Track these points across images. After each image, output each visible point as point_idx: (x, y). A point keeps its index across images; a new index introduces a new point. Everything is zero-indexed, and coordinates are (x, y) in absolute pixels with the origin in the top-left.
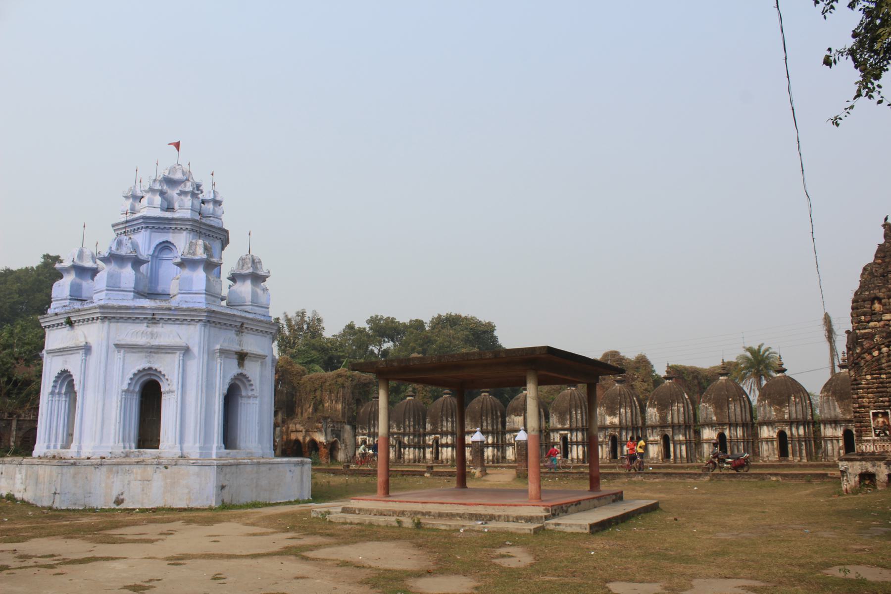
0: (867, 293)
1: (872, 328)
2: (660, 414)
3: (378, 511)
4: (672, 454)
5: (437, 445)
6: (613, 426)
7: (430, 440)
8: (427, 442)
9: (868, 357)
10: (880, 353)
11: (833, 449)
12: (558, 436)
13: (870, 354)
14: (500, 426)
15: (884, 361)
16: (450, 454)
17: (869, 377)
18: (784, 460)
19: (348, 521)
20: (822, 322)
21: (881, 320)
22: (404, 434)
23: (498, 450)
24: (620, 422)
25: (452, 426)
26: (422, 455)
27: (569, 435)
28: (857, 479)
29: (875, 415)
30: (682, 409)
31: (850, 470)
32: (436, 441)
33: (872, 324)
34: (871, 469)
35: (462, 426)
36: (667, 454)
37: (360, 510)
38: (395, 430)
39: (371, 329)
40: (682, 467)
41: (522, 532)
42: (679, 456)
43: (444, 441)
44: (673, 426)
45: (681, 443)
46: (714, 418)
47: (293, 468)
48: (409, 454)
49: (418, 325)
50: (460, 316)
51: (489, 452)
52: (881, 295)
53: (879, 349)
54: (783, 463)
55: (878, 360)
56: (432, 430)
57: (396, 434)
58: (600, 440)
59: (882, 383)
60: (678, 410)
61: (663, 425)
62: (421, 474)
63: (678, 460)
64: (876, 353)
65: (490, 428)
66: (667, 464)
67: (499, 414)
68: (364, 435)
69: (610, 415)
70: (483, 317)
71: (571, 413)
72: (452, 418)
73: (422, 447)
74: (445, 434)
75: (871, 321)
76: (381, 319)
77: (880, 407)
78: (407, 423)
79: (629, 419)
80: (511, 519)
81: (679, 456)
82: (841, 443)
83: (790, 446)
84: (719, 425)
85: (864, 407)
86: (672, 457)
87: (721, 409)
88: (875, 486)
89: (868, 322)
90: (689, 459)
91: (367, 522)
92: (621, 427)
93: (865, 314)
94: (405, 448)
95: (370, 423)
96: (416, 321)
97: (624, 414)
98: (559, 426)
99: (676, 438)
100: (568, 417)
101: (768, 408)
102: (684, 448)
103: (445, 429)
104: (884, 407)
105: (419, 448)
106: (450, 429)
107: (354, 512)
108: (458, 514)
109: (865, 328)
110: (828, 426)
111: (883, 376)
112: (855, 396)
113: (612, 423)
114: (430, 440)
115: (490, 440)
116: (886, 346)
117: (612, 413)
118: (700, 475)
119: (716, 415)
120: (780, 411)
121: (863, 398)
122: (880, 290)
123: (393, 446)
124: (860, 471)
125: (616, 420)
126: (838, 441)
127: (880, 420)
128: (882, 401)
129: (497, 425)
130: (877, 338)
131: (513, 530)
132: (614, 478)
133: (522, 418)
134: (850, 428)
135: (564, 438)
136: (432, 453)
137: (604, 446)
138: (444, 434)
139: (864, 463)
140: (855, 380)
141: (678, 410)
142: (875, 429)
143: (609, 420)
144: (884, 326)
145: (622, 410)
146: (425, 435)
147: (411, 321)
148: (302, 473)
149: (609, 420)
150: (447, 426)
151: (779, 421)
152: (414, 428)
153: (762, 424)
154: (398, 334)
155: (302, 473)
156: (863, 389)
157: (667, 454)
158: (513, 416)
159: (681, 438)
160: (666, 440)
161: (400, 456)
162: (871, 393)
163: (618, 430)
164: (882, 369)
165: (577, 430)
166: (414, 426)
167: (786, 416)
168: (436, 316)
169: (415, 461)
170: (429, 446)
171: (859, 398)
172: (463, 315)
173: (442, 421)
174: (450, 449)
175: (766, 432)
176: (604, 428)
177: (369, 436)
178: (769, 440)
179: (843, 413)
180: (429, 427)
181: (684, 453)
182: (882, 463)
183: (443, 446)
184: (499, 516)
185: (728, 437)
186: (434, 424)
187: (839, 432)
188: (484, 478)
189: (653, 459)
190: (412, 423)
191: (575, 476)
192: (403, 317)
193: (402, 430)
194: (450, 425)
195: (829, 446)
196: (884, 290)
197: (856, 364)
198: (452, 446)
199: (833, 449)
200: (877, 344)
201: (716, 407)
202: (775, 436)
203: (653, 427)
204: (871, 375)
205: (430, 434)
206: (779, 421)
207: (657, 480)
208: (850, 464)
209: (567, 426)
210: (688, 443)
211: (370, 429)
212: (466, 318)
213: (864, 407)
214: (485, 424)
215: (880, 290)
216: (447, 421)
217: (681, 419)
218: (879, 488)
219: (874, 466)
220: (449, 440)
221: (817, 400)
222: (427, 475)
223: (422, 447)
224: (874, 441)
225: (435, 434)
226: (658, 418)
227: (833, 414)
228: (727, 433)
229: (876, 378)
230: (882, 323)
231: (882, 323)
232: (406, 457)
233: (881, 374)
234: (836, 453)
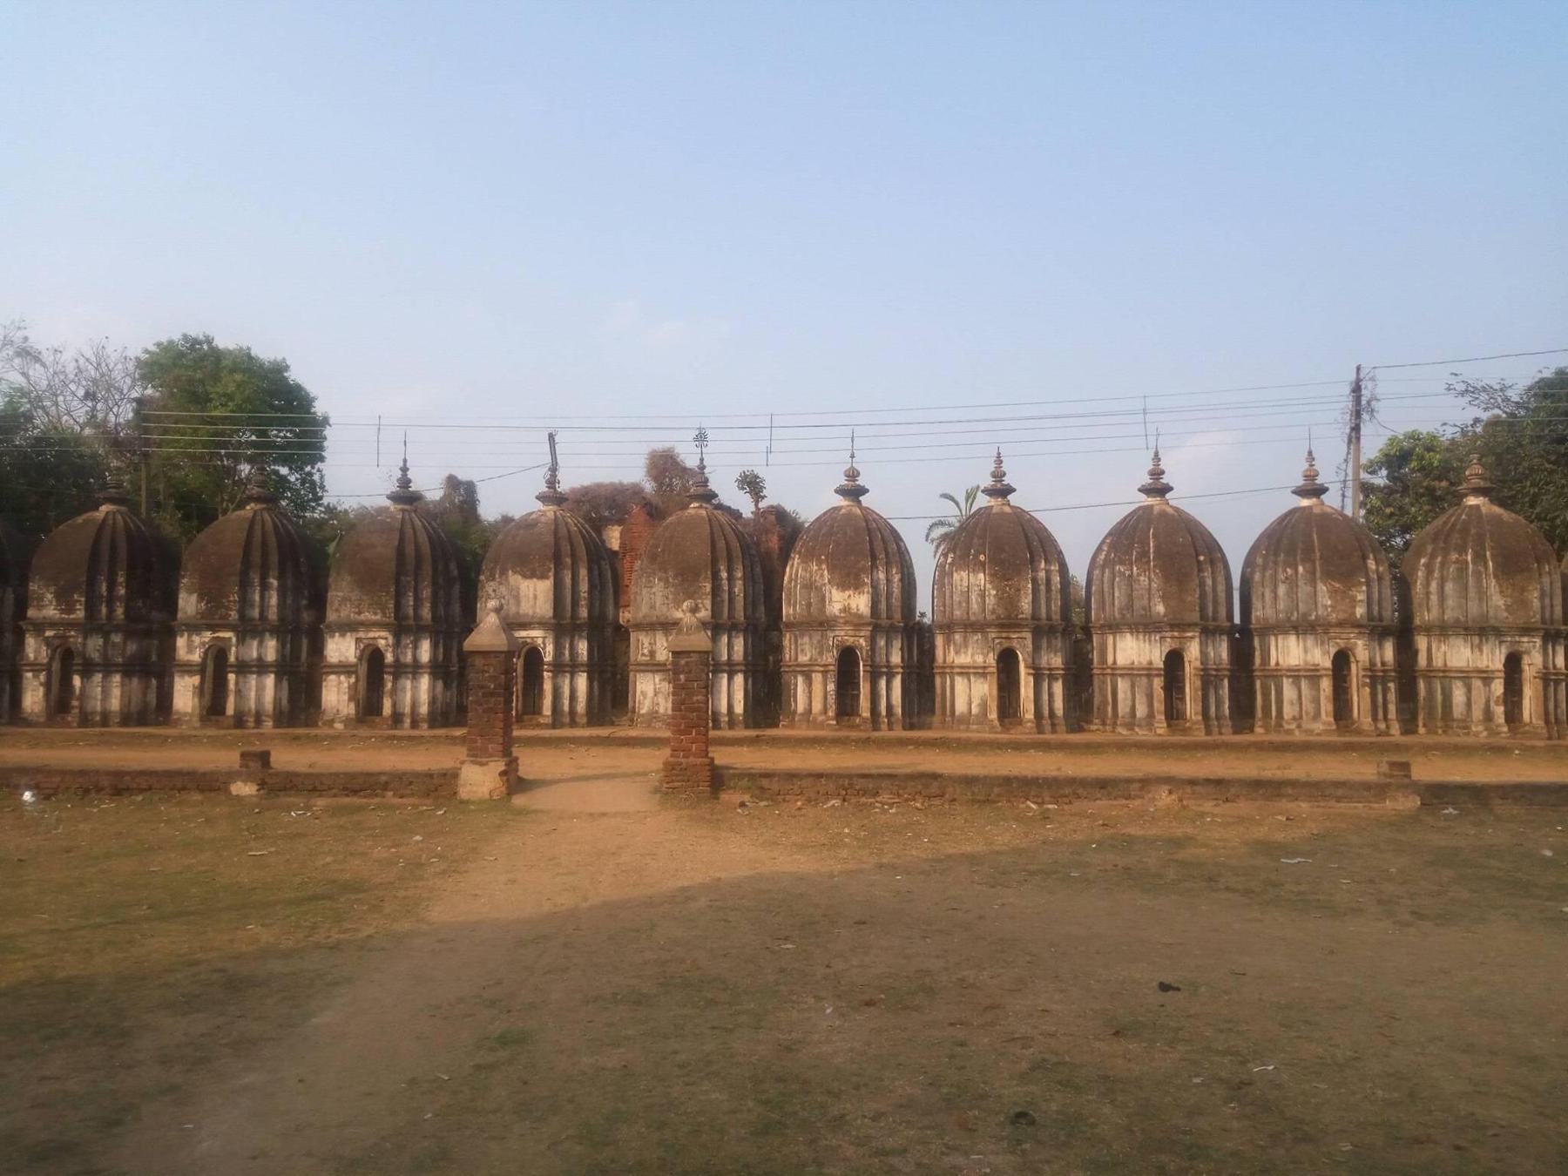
14: (457, 608)
20: (1347, 390)
23: (447, 686)
26: (152, 698)
38: (51, 612)
56: (203, 615)
57: (53, 624)
62: (210, 784)
65: (426, 612)
69: (843, 586)
71: (715, 577)
72: (280, 578)
84: (1173, 627)
101: (1304, 589)
113: (846, 609)
115: (1454, 556)
119: (1164, 598)
129: (448, 604)
136: (200, 690)
137: (817, 678)
138: (248, 629)
149: (838, 601)
158: (514, 579)
163: (866, 631)
165: (732, 628)
166: (129, 600)
167: (1360, 611)
173: (244, 585)
178: (343, 669)
181: (1059, 704)
183: (243, 668)
187: (1493, 658)
193: (80, 614)
195: (1459, 695)
198: (260, 659)
199: (1469, 704)
201: (1167, 578)
202: (1328, 664)
205: (194, 628)
206: (1340, 624)
210: (439, 670)
221: (925, 561)
225: (213, 628)
226: (991, 601)
227: (1474, 609)
234: (1477, 713)
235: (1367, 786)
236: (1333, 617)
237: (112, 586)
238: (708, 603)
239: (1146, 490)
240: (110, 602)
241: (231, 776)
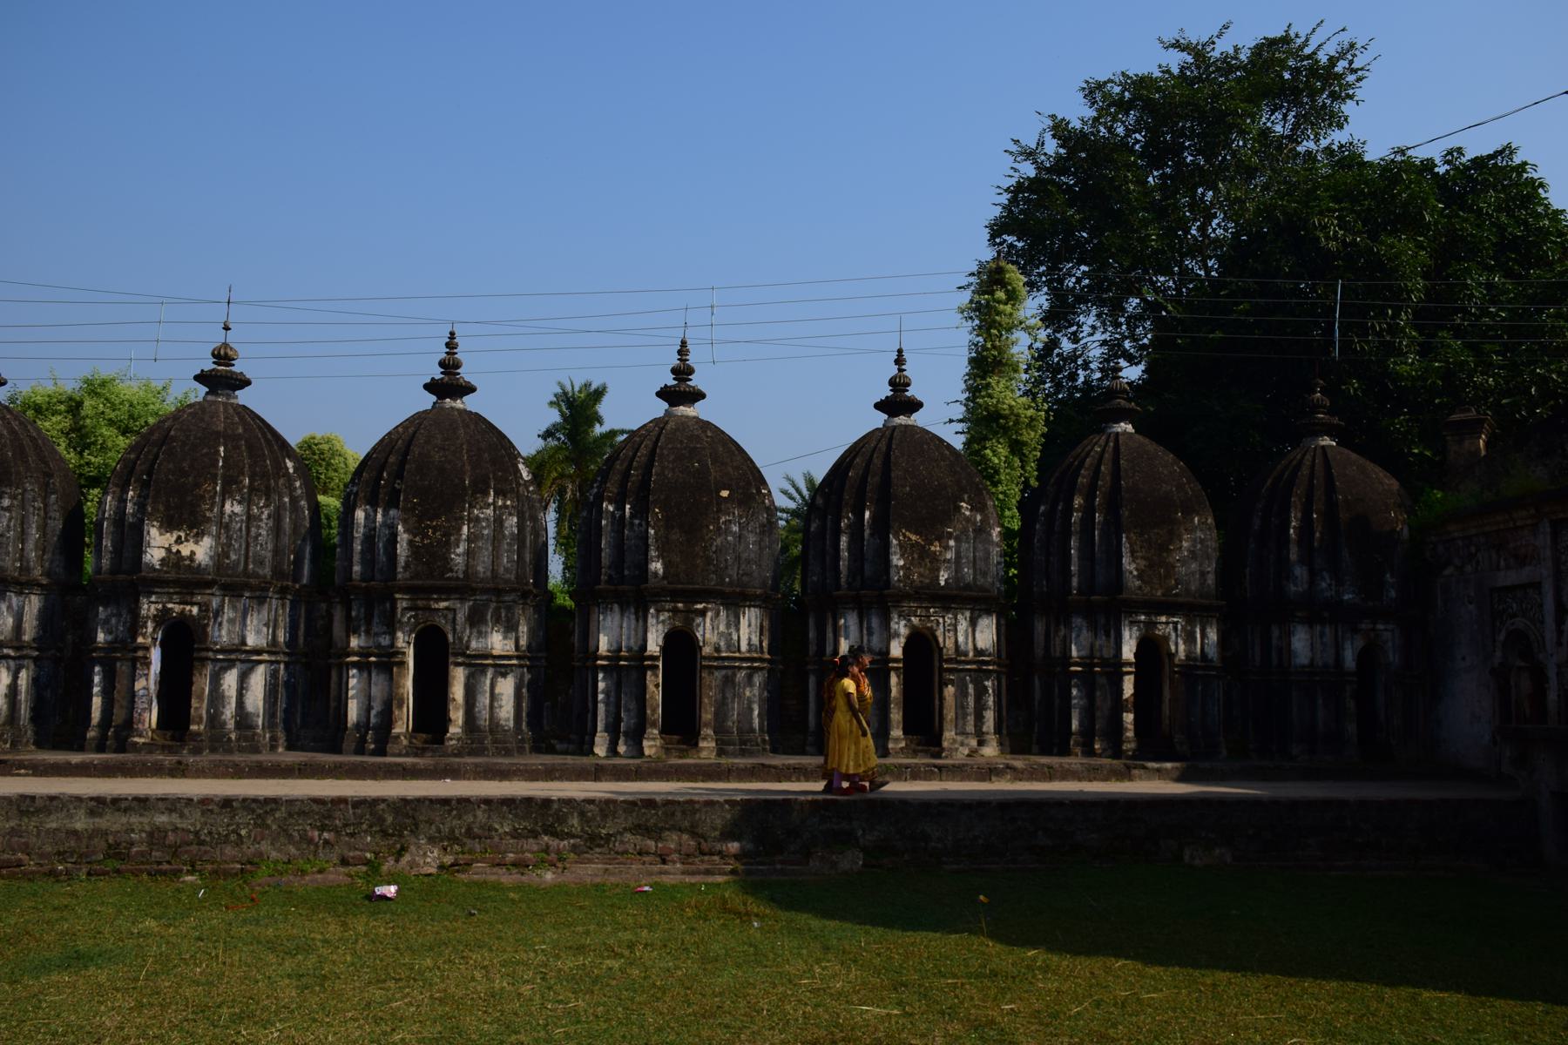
6: (182, 578)
44: (462, 588)
69: (168, 525)
84: (675, 595)
113: (173, 560)
125: (201, 550)
134: (1161, 630)
141: (499, 522)
159: (498, 642)
181: (506, 711)
239: (664, 394)
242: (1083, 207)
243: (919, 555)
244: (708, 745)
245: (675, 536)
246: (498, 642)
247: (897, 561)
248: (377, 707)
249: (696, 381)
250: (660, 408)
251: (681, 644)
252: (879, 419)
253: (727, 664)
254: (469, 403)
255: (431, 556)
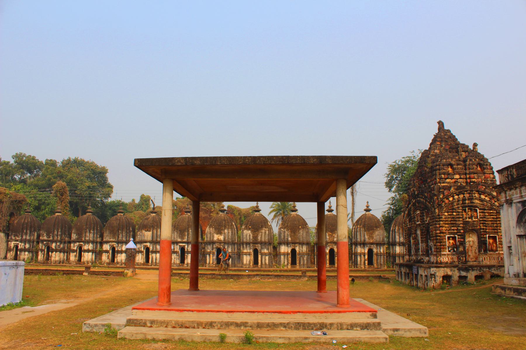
0: (445, 161)
1: (448, 183)
2: (253, 234)
3: (177, 323)
4: (260, 262)
5: (81, 250)
6: (220, 242)
7: (74, 246)
8: (72, 248)
9: (447, 201)
10: (454, 199)
11: (361, 261)
12: (178, 246)
13: (448, 199)
15: (455, 204)
16: (90, 257)
17: (446, 214)
18: (332, 267)
19: (150, 337)
21: (453, 178)
22: (52, 241)
24: (224, 239)
25: (94, 237)
26: (65, 257)
27: (186, 246)
28: (441, 279)
29: (449, 238)
30: (267, 232)
31: (437, 274)
32: (80, 248)
33: (448, 180)
34: (450, 273)
35: (102, 236)
36: (256, 262)
37: (152, 322)
38: (45, 238)
39: (16, 162)
40: (264, 271)
41: (377, 341)
42: (264, 263)
43: (86, 247)
44: (261, 243)
45: (265, 254)
46: (290, 239)
47: (7, 270)
48: (56, 257)
49: (52, 164)
50: (84, 161)
51: (140, 258)
52: (453, 162)
53: (453, 197)
54: (332, 269)
55: (452, 203)
56: (77, 239)
57: (46, 241)
58: (209, 251)
59: (453, 218)
60: (265, 233)
61: (255, 242)
62: (81, 273)
63: (264, 266)
64: (451, 199)
66: (256, 269)
67: (131, 229)
68: (17, 241)
69: (217, 234)
70: (100, 163)
71: (188, 231)
72: (94, 230)
73: (67, 251)
74: (88, 242)
75: (448, 178)
76: (24, 156)
77: (451, 233)
78: (56, 233)
79: (230, 237)
80: (345, 327)
81: (264, 263)
82: (366, 257)
83: (336, 258)
84: (293, 243)
85: (443, 233)
86: (260, 264)
87: (294, 233)
88: (450, 285)
89: (446, 179)
90: (270, 265)
91: (177, 338)
92: (225, 242)
93: (444, 174)
94: (52, 252)
95: (23, 232)
96: (51, 160)
97: (227, 234)
98: (179, 240)
99: (262, 251)
100: (186, 233)
102: (267, 258)
103: (87, 239)
104: (454, 234)
105: (64, 252)
106: (91, 239)
107: (144, 325)
108: (281, 324)
109: (444, 183)
110: (359, 246)
111: (454, 214)
112: (438, 226)
113: (218, 239)
114: (74, 246)
116: (457, 195)
117: (219, 232)
118: (300, 276)
119: (291, 237)
120: (332, 236)
121: (443, 227)
122: (452, 159)
123: (42, 250)
124: (443, 274)
125: (222, 238)
126: (364, 256)
127: (451, 241)
128: (453, 230)
130: (452, 189)
131: (366, 340)
132: (238, 279)
133: (151, 232)
135: (113, 249)
136: (76, 256)
137: (211, 255)
139: (446, 269)
140: (439, 215)
141: (265, 233)
142: (448, 247)
143: (216, 237)
144: (455, 182)
145: (226, 231)
146: (70, 242)
147: (47, 160)
148: (16, 275)
149: (216, 237)
150: (90, 236)
151: (331, 242)
152: (61, 237)
153: (280, 244)
154: (35, 169)
155: (16, 275)
156: (442, 221)
157: (256, 262)
158: (144, 231)
159: (266, 251)
160: (256, 252)
161: (48, 258)
162: (447, 224)
164: (453, 209)
166: (61, 235)
168: (66, 159)
169: (60, 263)
170: (74, 251)
171: (440, 227)
172: (86, 160)
173: (86, 232)
174: (90, 254)
175: (284, 249)
176: (213, 243)
177: (21, 242)
179: (369, 239)
180: (74, 236)
181: (267, 262)
182: (456, 269)
183: (86, 251)
184: (331, 324)
185: (298, 252)
186: (79, 234)
188: (135, 277)
189: (246, 265)
190: (60, 233)
191: (209, 276)
192: (42, 158)
194: (92, 235)
196: (454, 160)
197: (439, 205)
199: (361, 261)
200: (452, 193)
201: (291, 232)
202: (289, 252)
203: (248, 244)
204: (448, 212)
205: (75, 242)
206: (331, 242)
207: (270, 280)
208: (438, 269)
209: (185, 240)
211: (22, 237)
212: (88, 162)
213: (443, 233)
214: (120, 236)
215: (452, 159)
216: (90, 232)
217: (267, 238)
218: (453, 285)
219: (451, 271)
220: (90, 246)
222: (85, 274)
223: (67, 251)
224: (448, 254)
225: (79, 242)
226: (251, 237)
228: (297, 249)
229: (450, 215)
230: (453, 180)
231: (453, 180)
232: (53, 259)
233: (453, 212)
235: (297, 276)
236: (329, 241)
237: (58, 233)
238: (186, 237)
240: (57, 236)
241: (83, 271)
242: (103, 168)
243: (331, 236)
244: (298, 267)
245: (293, 234)
246: (266, 251)
247: (328, 237)
248: (248, 261)
249: (370, 208)
250: (364, 212)
251: (293, 251)
252: (364, 212)
253: (302, 255)
254: (371, 212)
255: (255, 237)
